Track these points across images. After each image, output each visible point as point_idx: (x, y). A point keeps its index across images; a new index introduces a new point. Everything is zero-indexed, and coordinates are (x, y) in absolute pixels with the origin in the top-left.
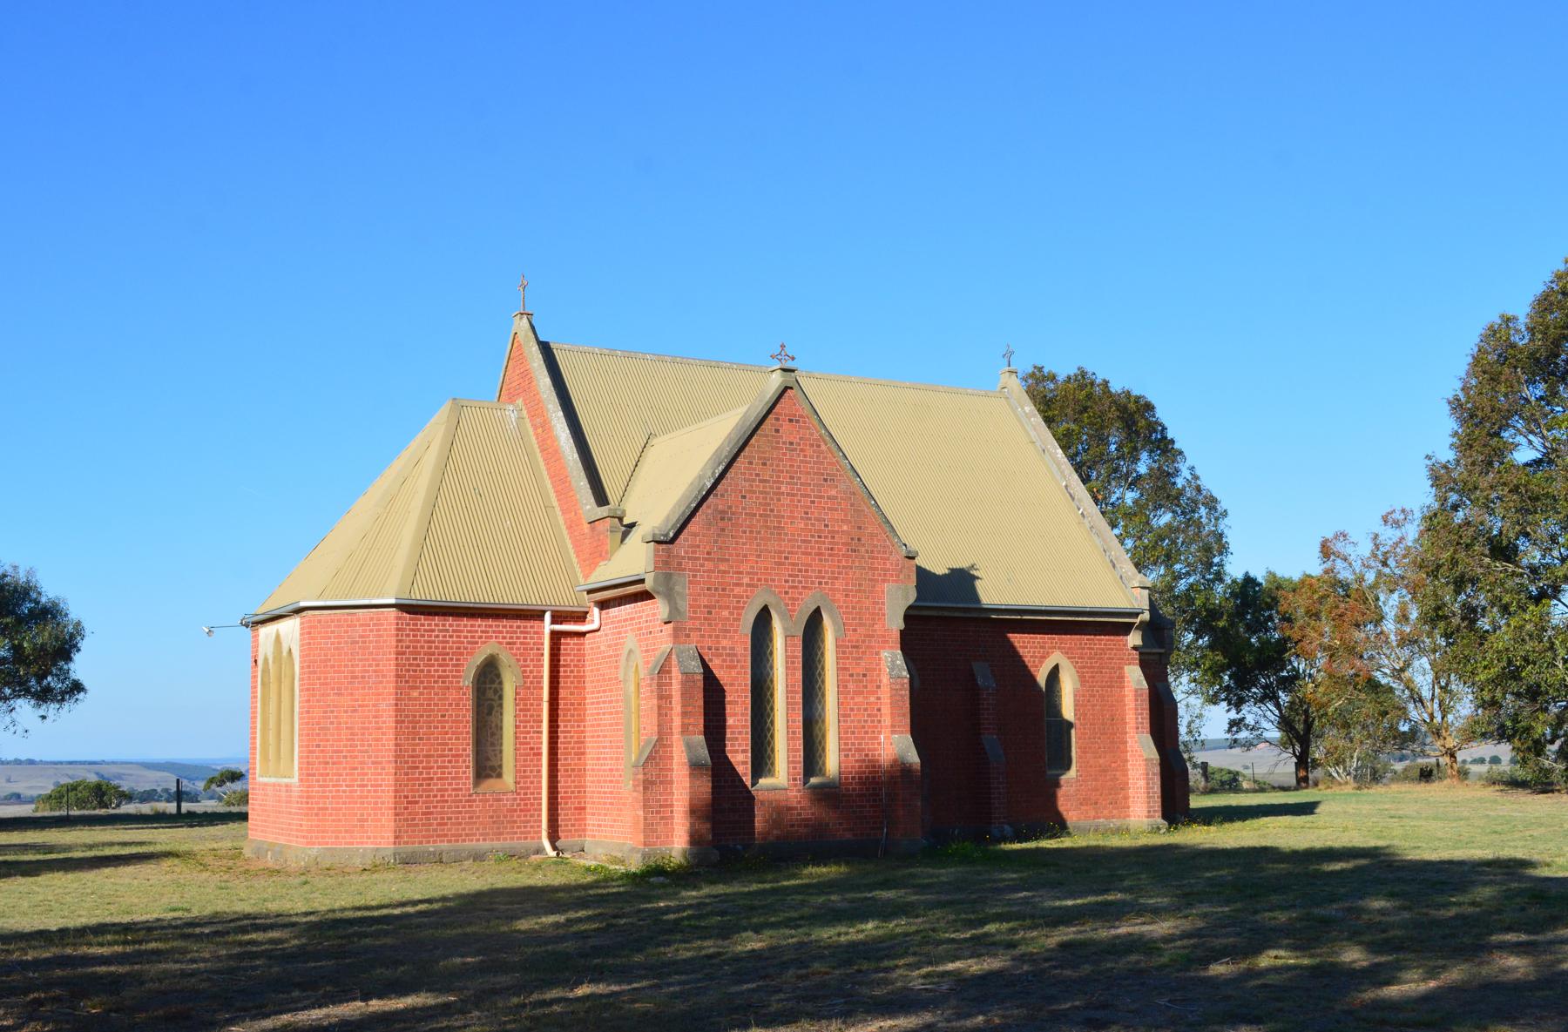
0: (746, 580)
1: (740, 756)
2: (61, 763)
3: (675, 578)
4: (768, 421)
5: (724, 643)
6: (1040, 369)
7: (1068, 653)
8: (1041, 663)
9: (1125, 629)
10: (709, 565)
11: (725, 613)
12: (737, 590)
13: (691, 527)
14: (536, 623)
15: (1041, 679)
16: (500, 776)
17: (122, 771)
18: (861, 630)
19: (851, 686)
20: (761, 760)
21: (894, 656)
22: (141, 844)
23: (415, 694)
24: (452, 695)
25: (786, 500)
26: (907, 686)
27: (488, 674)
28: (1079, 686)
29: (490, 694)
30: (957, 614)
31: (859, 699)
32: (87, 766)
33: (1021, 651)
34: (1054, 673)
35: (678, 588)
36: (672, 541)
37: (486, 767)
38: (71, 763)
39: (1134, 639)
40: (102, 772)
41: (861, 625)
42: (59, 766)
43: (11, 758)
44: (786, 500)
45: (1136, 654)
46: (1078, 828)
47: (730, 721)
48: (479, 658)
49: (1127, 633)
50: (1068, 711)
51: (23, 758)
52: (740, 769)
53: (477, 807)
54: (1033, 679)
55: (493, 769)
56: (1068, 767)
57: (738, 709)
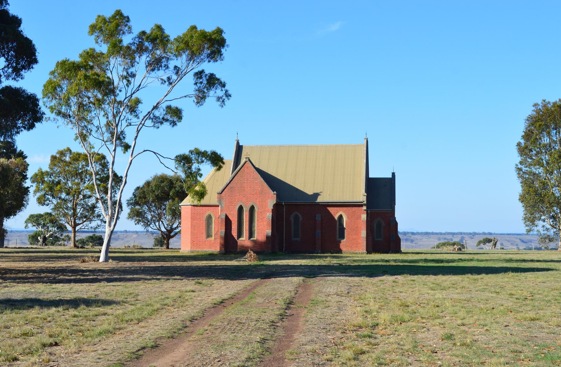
0: (237, 200)
1: (234, 233)
2: (504, 234)
3: (222, 200)
4: (242, 169)
5: (232, 212)
6: (544, 101)
7: (344, 212)
8: (336, 214)
9: (362, 206)
10: (228, 198)
11: (232, 207)
12: (235, 202)
13: (225, 190)
14: (218, 208)
15: (336, 217)
16: (212, 237)
17: (532, 239)
18: (262, 209)
19: (260, 221)
20: (240, 234)
21: (270, 214)
22: (442, 261)
23: (195, 221)
24: (202, 221)
25: (246, 184)
26: (271, 221)
27: (209, 217)
28: (347, 219)
29: (210, 221)
30: (307, 204)
31: (261, 223)
32: (516, 236)
33: (331, 211)
34: (341, 217)
35: (222, 202)
36: (221, 193)
37: (209, 235)
38: (509, 234)
39: (365, 208)
40: (521, 238)
41: (263, 208)
42: (503, 236)
43: (481, 232)
44: (246, 184)
45: (365, 212)
46: (345, 253)
47: (233, 227)
48: (207, 214)
49: (362, 207)
50: (345, 226)
51: (486, 232)
52: (235, 236)
53: (206, 243)
54: (334, 218)
55: (211, 236)
56: (344, 238)
57: (234, 225)
